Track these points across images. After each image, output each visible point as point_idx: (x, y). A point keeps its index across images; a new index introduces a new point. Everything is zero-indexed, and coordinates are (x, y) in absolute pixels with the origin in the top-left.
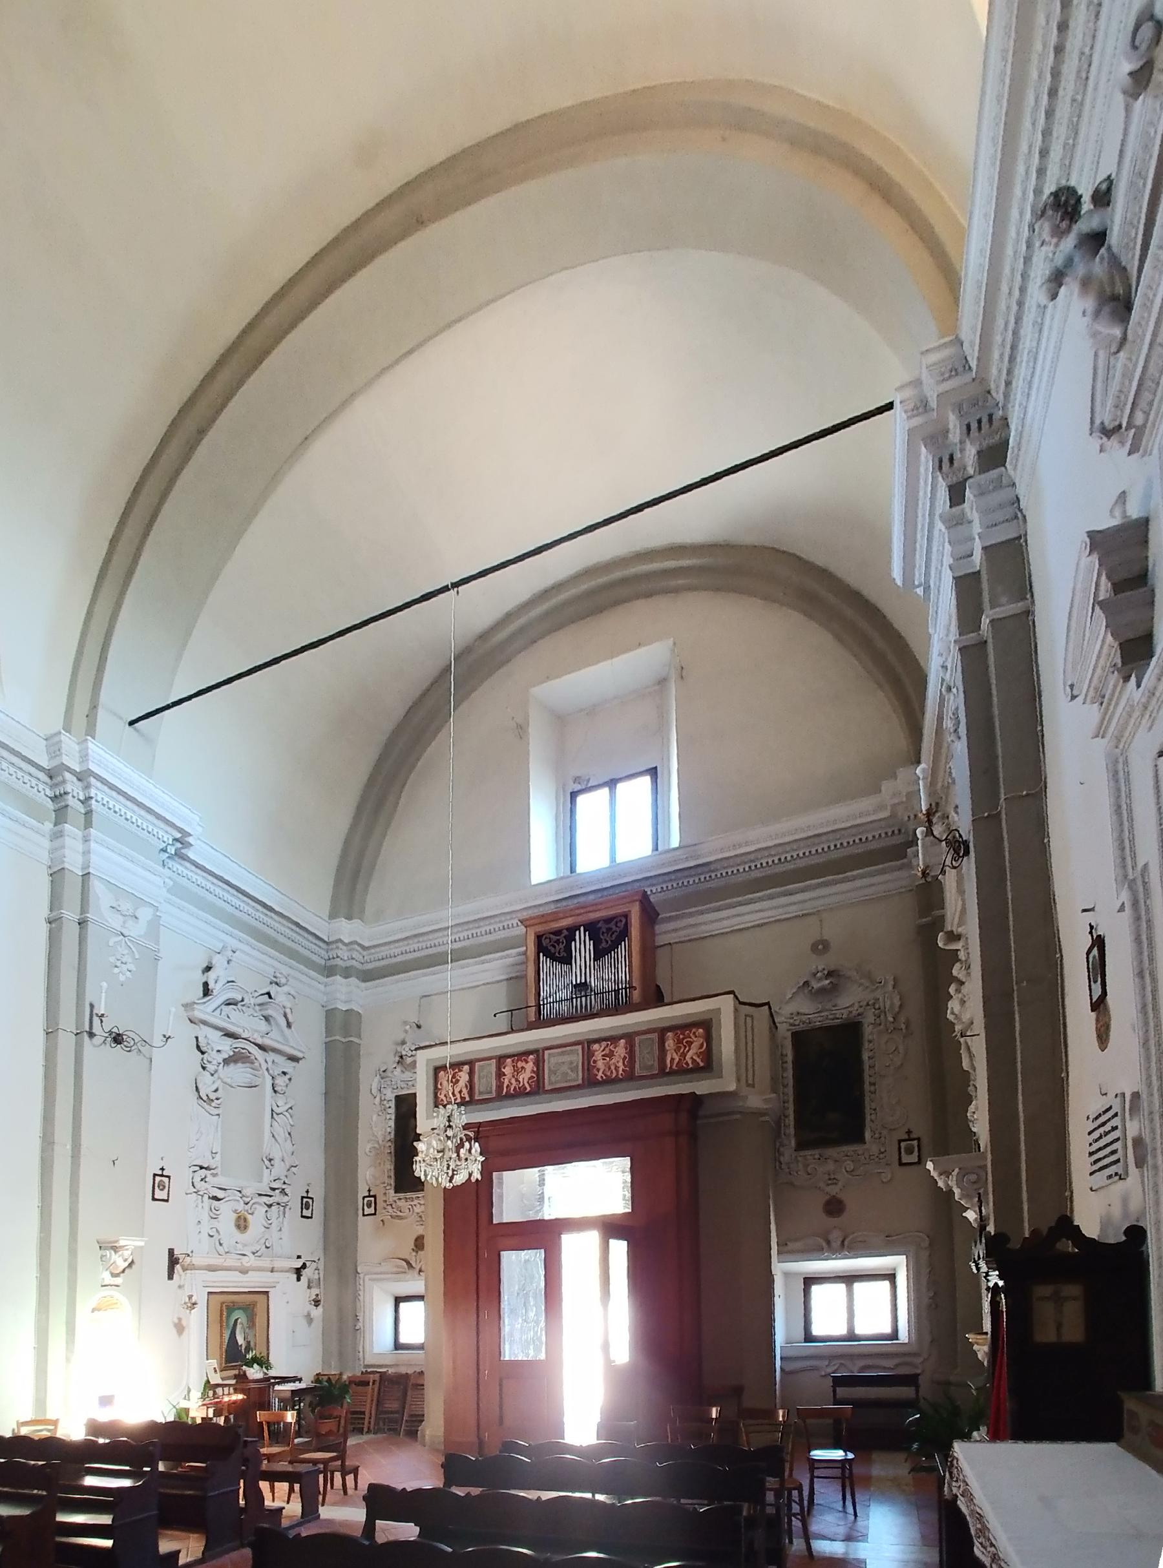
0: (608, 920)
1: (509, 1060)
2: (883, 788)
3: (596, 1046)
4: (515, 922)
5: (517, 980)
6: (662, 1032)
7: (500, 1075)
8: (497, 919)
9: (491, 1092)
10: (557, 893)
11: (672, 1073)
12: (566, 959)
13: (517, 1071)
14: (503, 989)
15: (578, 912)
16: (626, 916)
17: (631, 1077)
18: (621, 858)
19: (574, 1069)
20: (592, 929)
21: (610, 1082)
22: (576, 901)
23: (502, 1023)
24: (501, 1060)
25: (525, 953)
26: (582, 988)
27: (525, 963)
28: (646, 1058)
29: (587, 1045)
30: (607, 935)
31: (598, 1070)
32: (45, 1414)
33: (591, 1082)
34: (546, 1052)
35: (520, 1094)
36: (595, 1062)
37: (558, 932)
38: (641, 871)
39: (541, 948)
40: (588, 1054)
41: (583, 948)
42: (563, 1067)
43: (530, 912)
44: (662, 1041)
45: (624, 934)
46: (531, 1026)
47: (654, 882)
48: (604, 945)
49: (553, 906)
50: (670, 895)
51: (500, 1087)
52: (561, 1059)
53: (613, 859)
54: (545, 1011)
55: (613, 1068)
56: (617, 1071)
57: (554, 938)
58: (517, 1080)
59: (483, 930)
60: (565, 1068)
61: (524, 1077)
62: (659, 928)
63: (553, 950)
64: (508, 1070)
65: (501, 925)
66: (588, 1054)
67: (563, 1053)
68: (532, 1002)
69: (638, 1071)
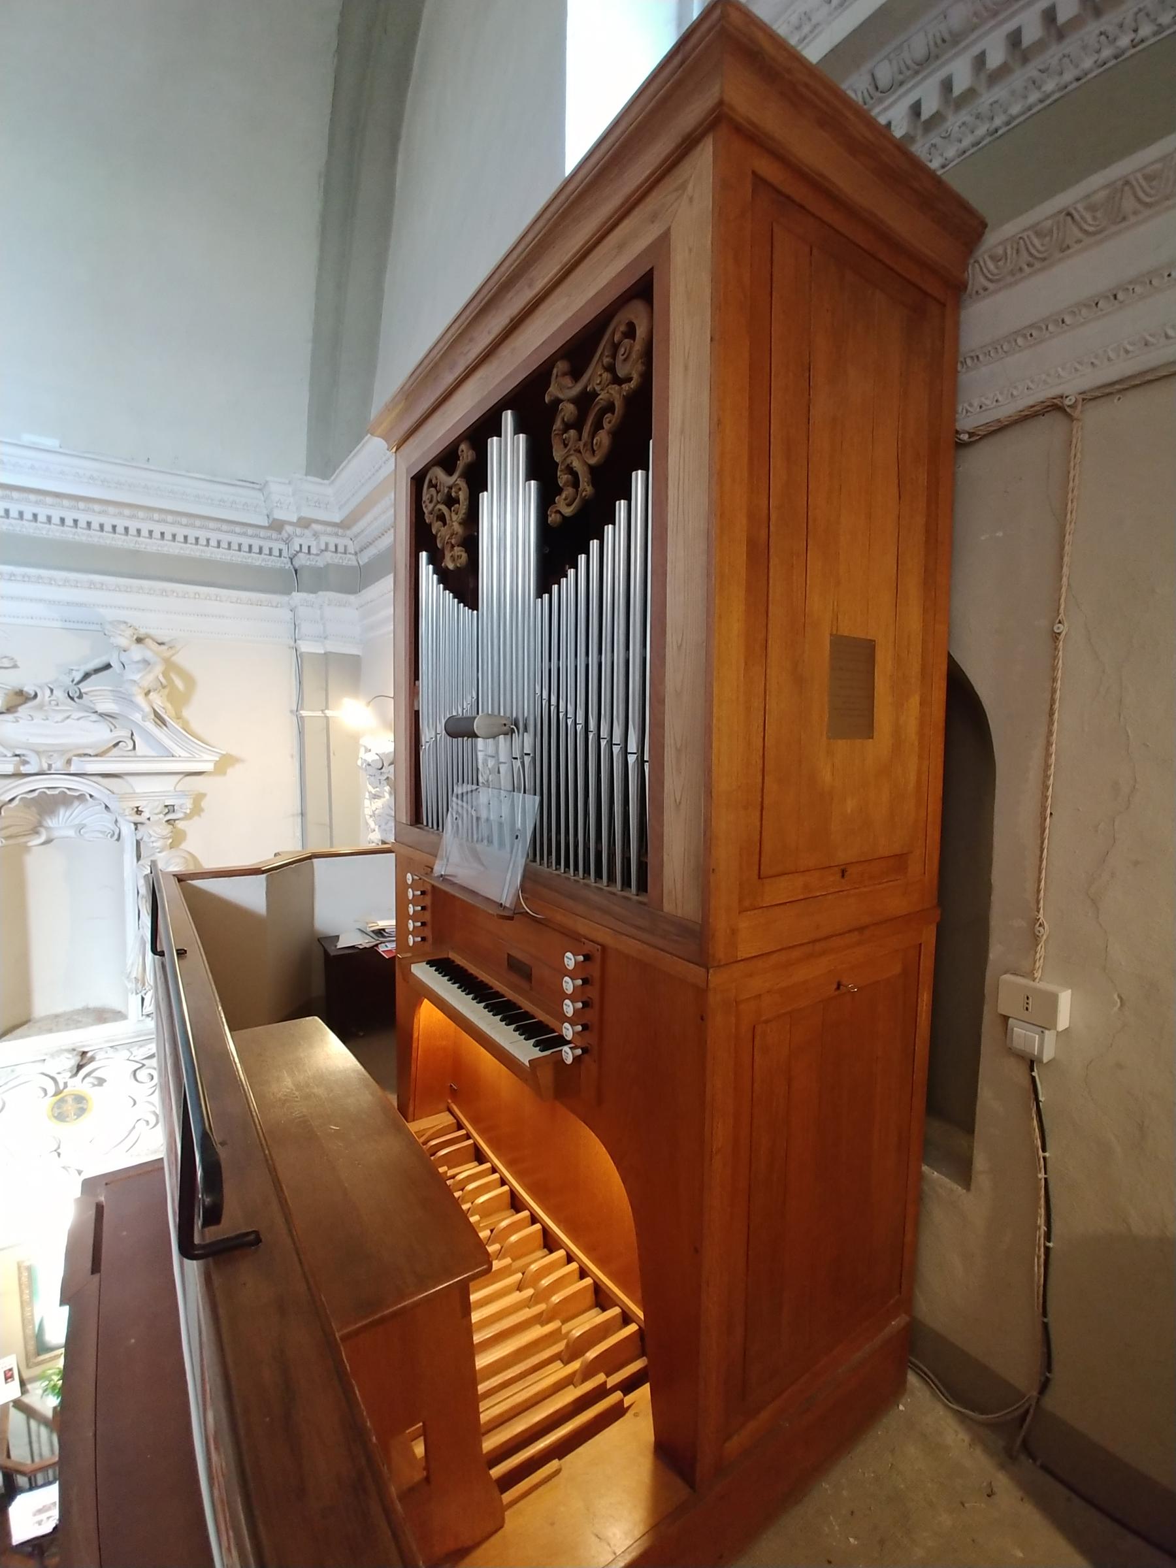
62: (985, 318)
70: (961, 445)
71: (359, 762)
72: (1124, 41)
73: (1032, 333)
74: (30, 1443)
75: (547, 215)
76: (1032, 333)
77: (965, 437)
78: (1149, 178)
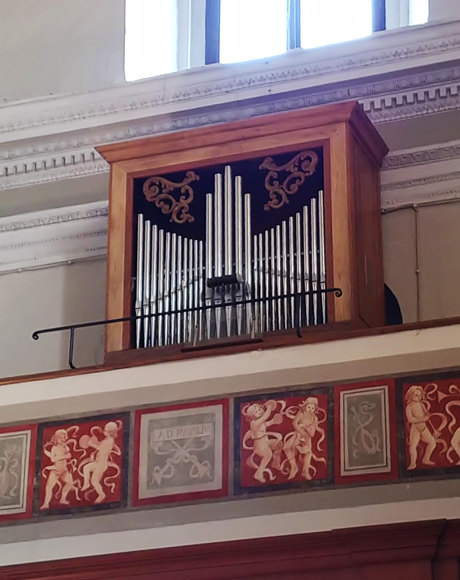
0: (281, 158)
1: (61, 433)
2: (193, 456)
3: (253, 409)
4: (88, 151)
5: (82, 265)
6: (399, 385)
7: (39, 463)
8: (52, 146)
9: (16, 501)
10: (177, 99)
11: (423, 473)
12: (195, 230)
13: (78, 455)
14: (56, 282)
15: (218, 138)
16: (320, 150)
17: (328, 478)
18: (311, 41)
19: (205, 456)
20: (250, 172)
21: (281, 486)
22: (215, 117)
23: (52, 351)
24: (43, 430)
25: (107, 213)
26: (225, 286)
27: (107, 232)
28: (363, 438)
29: (236, 405)
30: (279, 186)
31: (258, 459)
32: (333, 286)
33: (242, 486)
34: (145, 419)
35: (82, 506)
36: (251, 442)
37: (177, 176)
38: (351, 65)
39: (140, 204)
40: (237, 425)
41: (227, 204)
42: (179, 451)
43: (120, 134)
44: (398, 404)
45: (316, 183)
46: (113, 362)
47: (378, 88)
48: (273, 204)
49: (168, 125)
50: (412, 113)
51: (37, 492)
52: (174, 434)
53: (295, 41)
54: (145, 327)
55: (290, 456)
56: (300, 465)
57: (171, 185)
58: (76, 476)
59: (19, 163)
60: (183, 454)
61: (95, 470)
62: (388, 176)
63: (165, 209)
64: (58, 454)
65: (49, 160)
66: (237, 425)
67: (181, 421)
68: (118, 309)
69: (346, 468)
70: (383, 213)
71: (171, 221)
72: (425, 112)
73: (402, 184)
74: (41, 269)
75: (88, 371)
76: (402, 184)
77: (383, 211)
78: (432, 153)
